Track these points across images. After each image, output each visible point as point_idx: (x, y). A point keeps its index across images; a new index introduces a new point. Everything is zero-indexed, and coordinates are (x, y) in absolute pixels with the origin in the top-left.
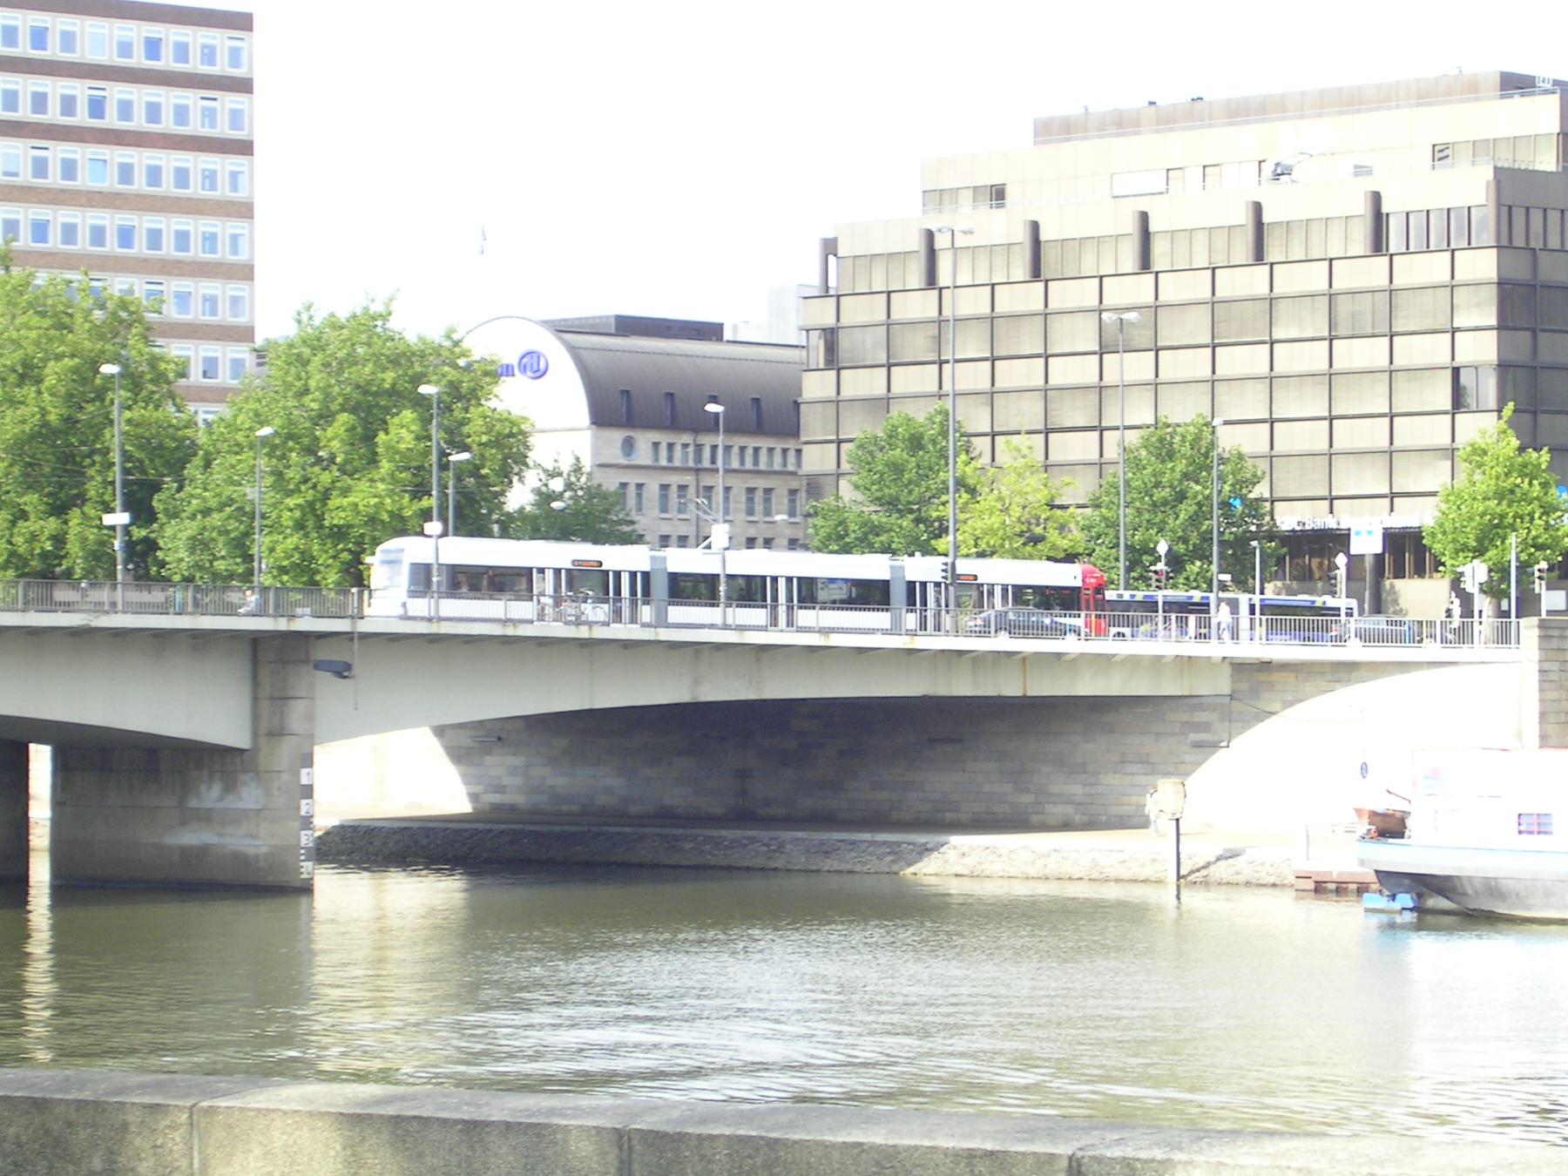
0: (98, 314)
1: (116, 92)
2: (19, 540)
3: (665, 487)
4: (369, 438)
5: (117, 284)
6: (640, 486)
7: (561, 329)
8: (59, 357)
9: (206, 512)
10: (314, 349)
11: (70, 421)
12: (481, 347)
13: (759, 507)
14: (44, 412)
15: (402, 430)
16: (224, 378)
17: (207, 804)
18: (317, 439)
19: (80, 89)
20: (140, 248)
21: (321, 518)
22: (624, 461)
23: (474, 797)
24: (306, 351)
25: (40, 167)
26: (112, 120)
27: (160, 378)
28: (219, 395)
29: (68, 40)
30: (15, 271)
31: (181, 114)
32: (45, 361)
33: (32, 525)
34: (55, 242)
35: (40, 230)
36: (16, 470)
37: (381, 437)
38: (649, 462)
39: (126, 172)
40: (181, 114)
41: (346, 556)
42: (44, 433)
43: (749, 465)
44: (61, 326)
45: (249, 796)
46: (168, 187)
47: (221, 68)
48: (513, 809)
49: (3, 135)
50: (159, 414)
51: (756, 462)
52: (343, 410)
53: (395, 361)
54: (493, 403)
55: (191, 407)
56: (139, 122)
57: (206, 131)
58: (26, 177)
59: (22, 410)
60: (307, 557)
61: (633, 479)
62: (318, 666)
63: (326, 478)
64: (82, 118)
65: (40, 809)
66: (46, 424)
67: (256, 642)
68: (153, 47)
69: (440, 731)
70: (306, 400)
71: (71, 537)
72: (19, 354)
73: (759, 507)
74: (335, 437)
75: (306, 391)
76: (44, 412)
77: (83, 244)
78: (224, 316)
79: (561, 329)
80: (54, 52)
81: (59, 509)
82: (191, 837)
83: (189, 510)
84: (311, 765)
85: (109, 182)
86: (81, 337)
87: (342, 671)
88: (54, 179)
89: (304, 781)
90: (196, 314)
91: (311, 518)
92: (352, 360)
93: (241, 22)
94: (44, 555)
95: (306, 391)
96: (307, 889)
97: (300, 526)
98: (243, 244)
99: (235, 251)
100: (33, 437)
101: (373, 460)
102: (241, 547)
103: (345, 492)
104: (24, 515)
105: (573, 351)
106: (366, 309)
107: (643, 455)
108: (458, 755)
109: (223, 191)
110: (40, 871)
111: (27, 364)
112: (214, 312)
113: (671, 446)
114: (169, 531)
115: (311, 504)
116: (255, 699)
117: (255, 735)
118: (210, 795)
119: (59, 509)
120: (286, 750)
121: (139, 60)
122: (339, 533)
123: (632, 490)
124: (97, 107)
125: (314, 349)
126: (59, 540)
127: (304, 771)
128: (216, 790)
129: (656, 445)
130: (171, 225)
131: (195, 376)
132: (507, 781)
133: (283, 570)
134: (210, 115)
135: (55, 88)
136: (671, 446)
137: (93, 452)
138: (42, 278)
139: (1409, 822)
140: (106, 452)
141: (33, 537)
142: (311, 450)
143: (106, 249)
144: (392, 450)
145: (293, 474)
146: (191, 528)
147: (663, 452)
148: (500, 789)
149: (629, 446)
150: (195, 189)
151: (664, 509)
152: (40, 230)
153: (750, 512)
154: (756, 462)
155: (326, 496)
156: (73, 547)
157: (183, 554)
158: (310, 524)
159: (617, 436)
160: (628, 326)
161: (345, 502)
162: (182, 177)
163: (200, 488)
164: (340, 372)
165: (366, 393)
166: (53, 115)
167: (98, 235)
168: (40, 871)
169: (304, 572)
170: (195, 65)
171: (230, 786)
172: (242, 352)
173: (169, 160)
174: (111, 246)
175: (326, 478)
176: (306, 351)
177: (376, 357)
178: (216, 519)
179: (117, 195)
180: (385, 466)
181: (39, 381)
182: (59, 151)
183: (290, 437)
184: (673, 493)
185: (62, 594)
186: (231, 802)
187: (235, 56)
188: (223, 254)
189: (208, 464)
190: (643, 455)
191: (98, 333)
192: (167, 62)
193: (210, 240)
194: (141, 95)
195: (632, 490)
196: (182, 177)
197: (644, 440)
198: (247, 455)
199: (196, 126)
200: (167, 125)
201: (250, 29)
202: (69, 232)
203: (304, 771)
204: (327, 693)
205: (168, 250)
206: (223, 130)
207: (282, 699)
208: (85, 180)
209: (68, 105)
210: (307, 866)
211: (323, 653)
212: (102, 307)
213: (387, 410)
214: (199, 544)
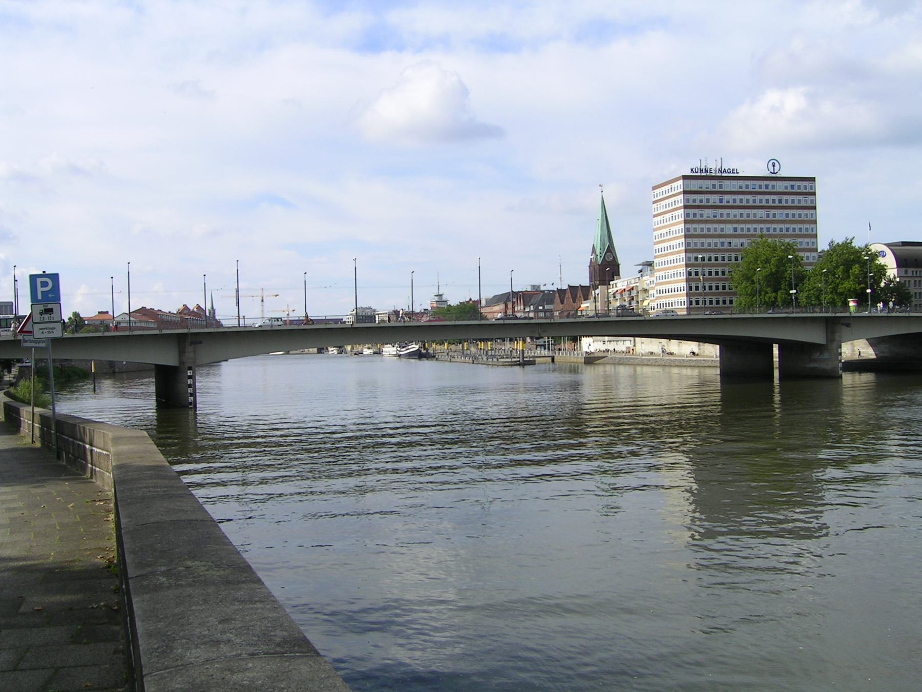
0: (783, 247)
1: (784, 197)
2: (766, 298)
3: (915, 281)
4: (848, 272)
5: (787, 240)
6: (909, 281)
7: (888, 245)
8: (775, 257)
9: (809, 290)
10: (834, 252)
11: (777, 271)
12: (874, 248)
13: (917, 285)
14: (771, 269)
15: (856, 269)
16: (811, 260)
17: (815, 358)
18: (835, 272)
19: (776, 197)
20: (791, 232)
21: (836, 291)
22: (905, 275)
23: (876, 355)
24: (831, 252)
25: (768, 216)
26: (784, 204)
27: (797, 261)
28: (811, 264)
29: (773, 187)
30: (764, 239)
31: (799, 201)
32: (771, 258)
33: (769, 295)
34: (771, 232)
35: (768, 229)
36: (766, 283)
37: (851, 271)
38: (911, 275)
39: (787, 215)
40: (799, 201)
41: (843, 299)
42: (772, 274)
43: (918, 275)
44: (774, 250)
45: (826, 356)
46: (797, 218)
47: (808, 190)
48: (886, 357)
49: (2, 486)
50: (798, 269)
51: (916, 274)
52: (841, 265)
53: (853, 253)
54: (877, 262)
55: (805, 267)
56: (790, 204)
57: (805, 205)
58: (765, 218)
59: (766, 270)
60: (833, 299)
61: (907, 279)
62: (843, 324)
63: (838, 281)
64: (777, 204)
65: (776, 359)
66: (772, 272)
67: (827, 319)
68: (792, 187)
69: (867, 340)
70: (832, 263)
71: (779, 297)
72: (765, 257)
73: (917, 285)
74: (840, 272)
75: (832, 261)
76: (771, 269)
77: (778, 232)
78: (810, 246)
79: (888, 245)
80: (770, 189)
81: (776, 291)
82: (812, 365)
83: (805, 290)
84: (841, 348)
85: (784, 218)
86: (779, 252)
87: (848, 325)
88: (771, 218)
89: (839, 351)
90: (804, 246)
91: (835, 290)
92: (843, 253)
93: (813, 179)
94: (772, 302)
95: (832, 261)
96: (841, 377)
97: (831, 292)
98: (814, 230)
99: (812, 231)
100: (769, 275)
101: (849, 277)
102: (818, 298)
103: (842, 284)
104: (767, 293)
105: (892, 250)
106: (846, 242)
107: (910, 274)
108: (872, 345)
109: (809, 218)
110: (776, 373)
111: (767, 259)
112: (808, 245)
113: (916, 272)
114: (801, 295)
115: (834, 287)
116: (827, 333)
117: (827, 341)
118: (817, 355)
119: (776, 291)
120: (834, 345)
121: (789, 190)
122: (841, 294)
123: (907, 282)
124: (780, 201)
125: (834, 252)
126: (776, 298)
127: (839, 349)
128: (818, 354)
129: (913, 271)
130: (797, 226)
131: (805, 260)
132: (885, 350)
133: (828, 303)
134: (806, 201)
135: (771, 197)
136: (916, 272)
137: (783, 278)
138: (770, 240)
139: (533, 284)
140: (785, 278)
141: (770, 298)
142: (834, 275)
143: (783, 233)
144: (853, 274)
145: (830, 280)
146: (806, 294)
147: (915, 273)
148: (883, 353)
149: (906, 272)
150: (803, 218)
151: (915, 286)
152: (768, 229)
153: (915, 286)
154: (916, 274)
155: (838, 285)
156: (779, 299)
157: (804, 300)
158: (834, 291)
159: (903, 269)
160: (904, 244)
161: (842, 286)
162: (794, 215)
163: (807, 285)
164: (840, 256)
165: (847, 261)
166: (771, 204)
167: (781, 230)
168: (776, 373)
169: (833, 303)
170: (802, 190)
171: (821, 353)
172: (814, 254)
173: (797, 212)
174: (784, 232)
175: (838, 281)
176: (831, 252)
177: (849, 253)
178: (812, 292)
179: (785, 221)
180: (852, 278)
181: (770, 263)
182: (772, 211)
183: (829, 272)
184: (917, 282)
185: (777, 310)
186: (822, 357)
187: (811, 187)
188: (810, 232)
189: (809, 280)
190: (910, 274)
191: (783, 251)
192: (796, 190)
193: (807, 229)
194: (790, 198)
195: (907, 282)
196: (800, 215)
197: (910, 270)
198: (819, 277)
199: (803, 204)
200: (796, 204)
201: (815, 181)
202: (775, 229)
203: (839, 349)
204: (845, 331)
205: (797, 232)
206: (809, 204)
207: (833, 333)
208: (778, 218)
209: (774, 201)
210: (841, 371)
211: (843, 321)
212: (784, 245)
213: (852, 265)
214: (808, 298)
